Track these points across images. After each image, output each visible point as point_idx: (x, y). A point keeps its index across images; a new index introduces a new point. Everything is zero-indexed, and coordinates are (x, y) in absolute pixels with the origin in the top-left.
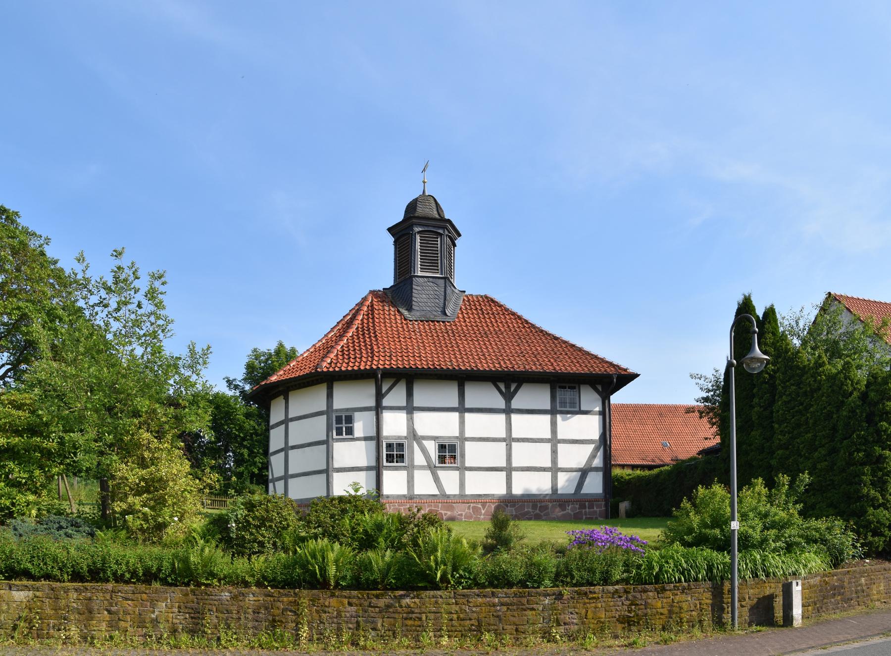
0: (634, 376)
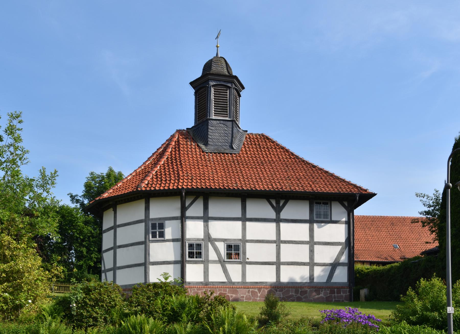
0: (372, 195)
